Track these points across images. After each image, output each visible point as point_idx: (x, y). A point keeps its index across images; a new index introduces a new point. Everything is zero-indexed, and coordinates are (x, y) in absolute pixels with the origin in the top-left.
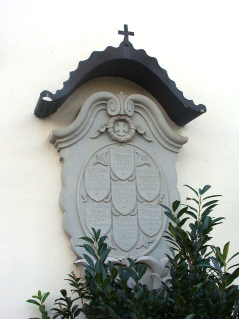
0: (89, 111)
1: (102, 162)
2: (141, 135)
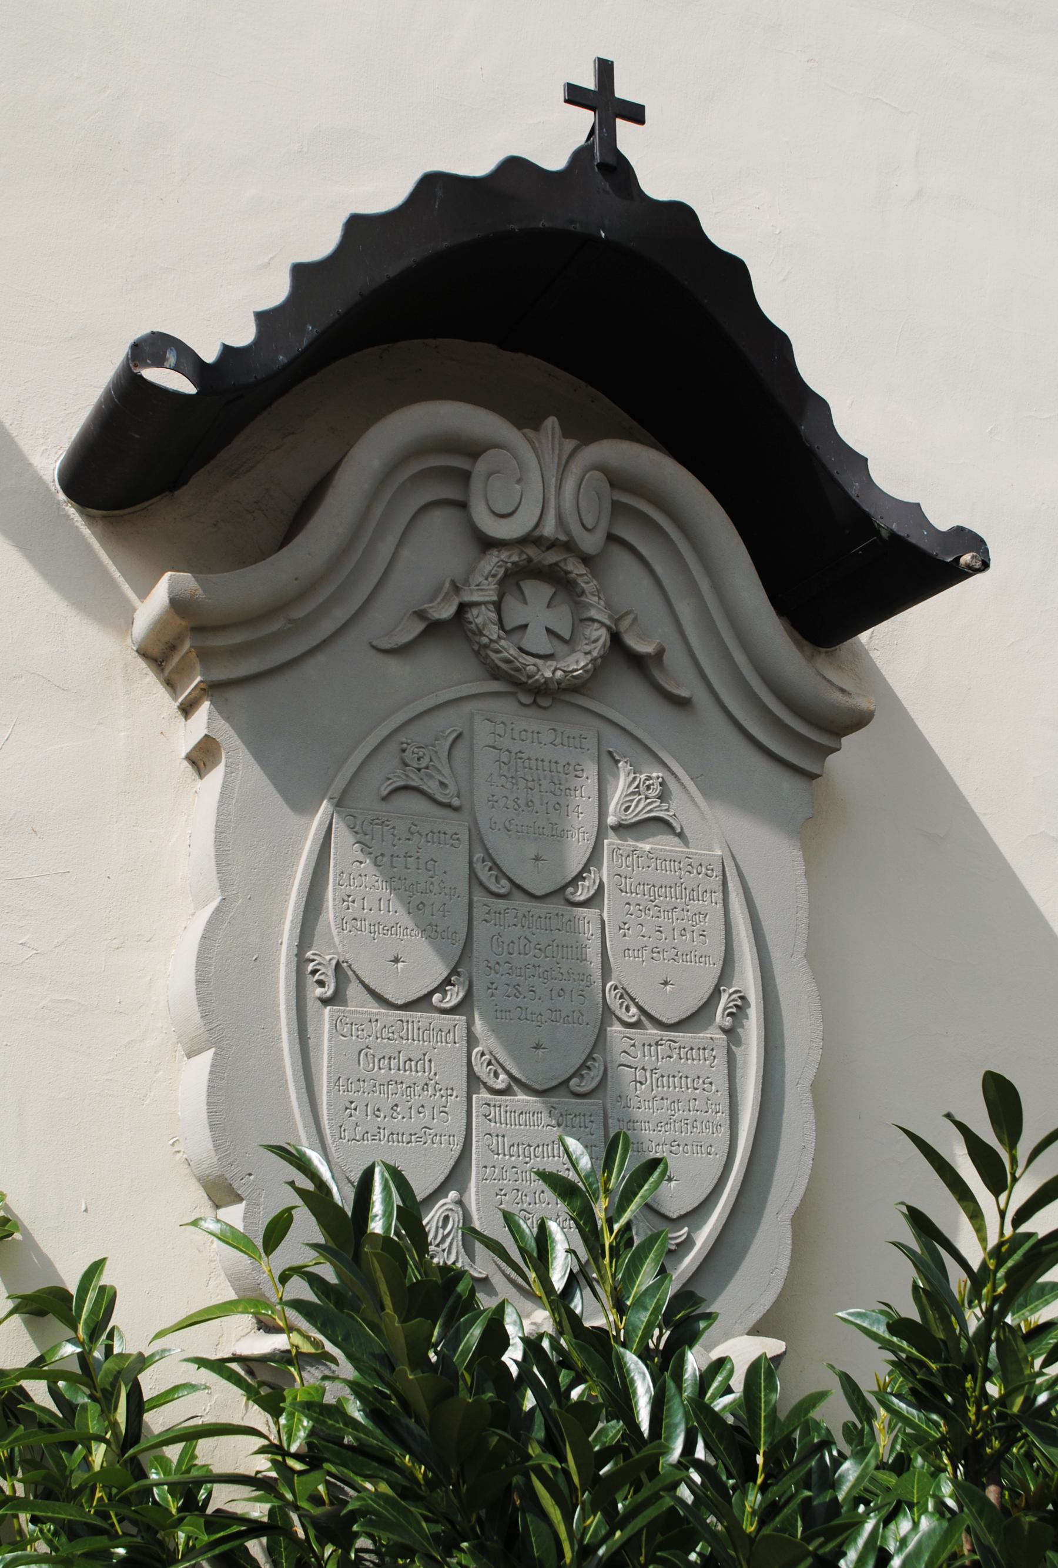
0: (375, 494)
1: (432, 787)
2: (638, 662)
